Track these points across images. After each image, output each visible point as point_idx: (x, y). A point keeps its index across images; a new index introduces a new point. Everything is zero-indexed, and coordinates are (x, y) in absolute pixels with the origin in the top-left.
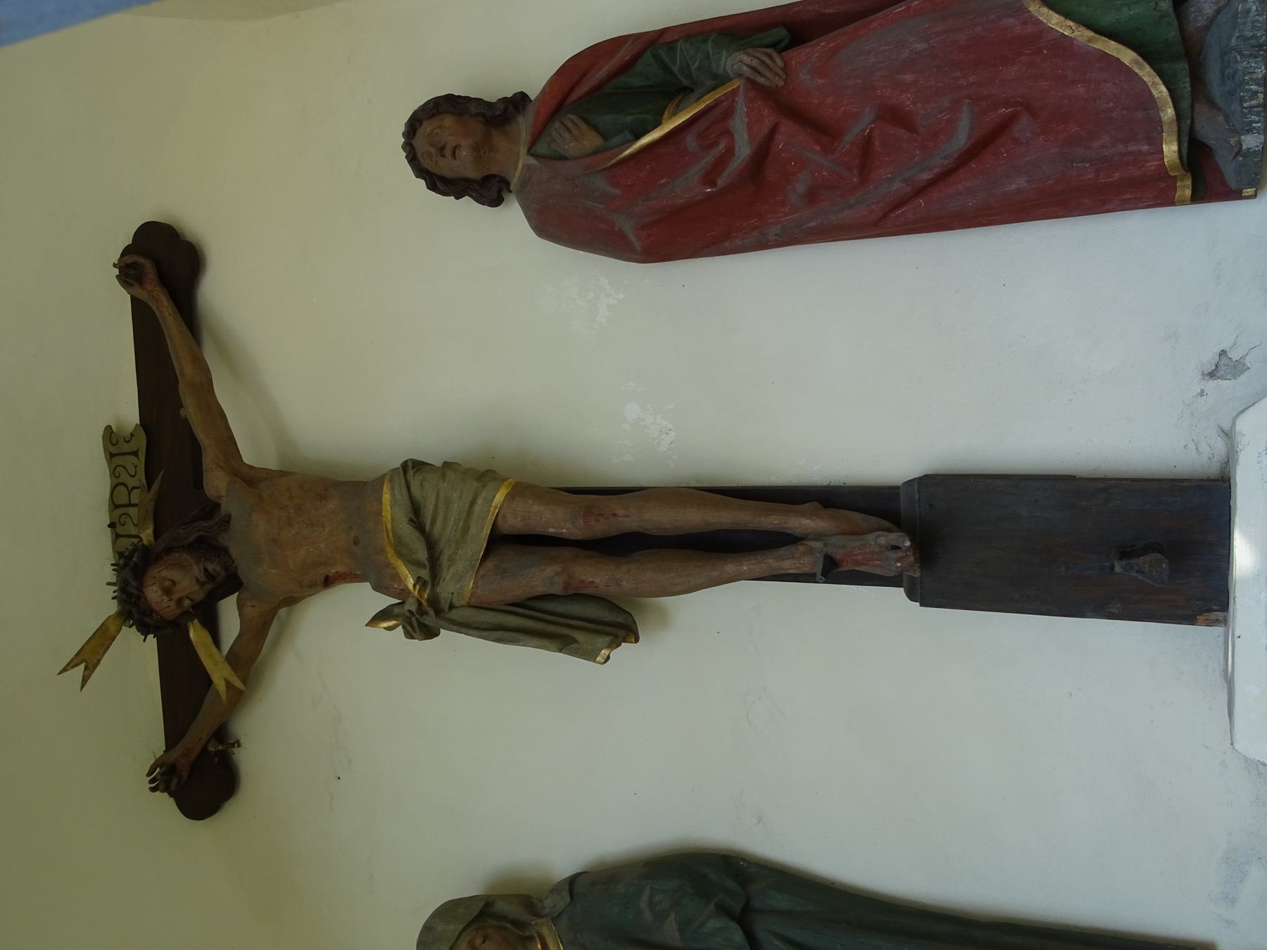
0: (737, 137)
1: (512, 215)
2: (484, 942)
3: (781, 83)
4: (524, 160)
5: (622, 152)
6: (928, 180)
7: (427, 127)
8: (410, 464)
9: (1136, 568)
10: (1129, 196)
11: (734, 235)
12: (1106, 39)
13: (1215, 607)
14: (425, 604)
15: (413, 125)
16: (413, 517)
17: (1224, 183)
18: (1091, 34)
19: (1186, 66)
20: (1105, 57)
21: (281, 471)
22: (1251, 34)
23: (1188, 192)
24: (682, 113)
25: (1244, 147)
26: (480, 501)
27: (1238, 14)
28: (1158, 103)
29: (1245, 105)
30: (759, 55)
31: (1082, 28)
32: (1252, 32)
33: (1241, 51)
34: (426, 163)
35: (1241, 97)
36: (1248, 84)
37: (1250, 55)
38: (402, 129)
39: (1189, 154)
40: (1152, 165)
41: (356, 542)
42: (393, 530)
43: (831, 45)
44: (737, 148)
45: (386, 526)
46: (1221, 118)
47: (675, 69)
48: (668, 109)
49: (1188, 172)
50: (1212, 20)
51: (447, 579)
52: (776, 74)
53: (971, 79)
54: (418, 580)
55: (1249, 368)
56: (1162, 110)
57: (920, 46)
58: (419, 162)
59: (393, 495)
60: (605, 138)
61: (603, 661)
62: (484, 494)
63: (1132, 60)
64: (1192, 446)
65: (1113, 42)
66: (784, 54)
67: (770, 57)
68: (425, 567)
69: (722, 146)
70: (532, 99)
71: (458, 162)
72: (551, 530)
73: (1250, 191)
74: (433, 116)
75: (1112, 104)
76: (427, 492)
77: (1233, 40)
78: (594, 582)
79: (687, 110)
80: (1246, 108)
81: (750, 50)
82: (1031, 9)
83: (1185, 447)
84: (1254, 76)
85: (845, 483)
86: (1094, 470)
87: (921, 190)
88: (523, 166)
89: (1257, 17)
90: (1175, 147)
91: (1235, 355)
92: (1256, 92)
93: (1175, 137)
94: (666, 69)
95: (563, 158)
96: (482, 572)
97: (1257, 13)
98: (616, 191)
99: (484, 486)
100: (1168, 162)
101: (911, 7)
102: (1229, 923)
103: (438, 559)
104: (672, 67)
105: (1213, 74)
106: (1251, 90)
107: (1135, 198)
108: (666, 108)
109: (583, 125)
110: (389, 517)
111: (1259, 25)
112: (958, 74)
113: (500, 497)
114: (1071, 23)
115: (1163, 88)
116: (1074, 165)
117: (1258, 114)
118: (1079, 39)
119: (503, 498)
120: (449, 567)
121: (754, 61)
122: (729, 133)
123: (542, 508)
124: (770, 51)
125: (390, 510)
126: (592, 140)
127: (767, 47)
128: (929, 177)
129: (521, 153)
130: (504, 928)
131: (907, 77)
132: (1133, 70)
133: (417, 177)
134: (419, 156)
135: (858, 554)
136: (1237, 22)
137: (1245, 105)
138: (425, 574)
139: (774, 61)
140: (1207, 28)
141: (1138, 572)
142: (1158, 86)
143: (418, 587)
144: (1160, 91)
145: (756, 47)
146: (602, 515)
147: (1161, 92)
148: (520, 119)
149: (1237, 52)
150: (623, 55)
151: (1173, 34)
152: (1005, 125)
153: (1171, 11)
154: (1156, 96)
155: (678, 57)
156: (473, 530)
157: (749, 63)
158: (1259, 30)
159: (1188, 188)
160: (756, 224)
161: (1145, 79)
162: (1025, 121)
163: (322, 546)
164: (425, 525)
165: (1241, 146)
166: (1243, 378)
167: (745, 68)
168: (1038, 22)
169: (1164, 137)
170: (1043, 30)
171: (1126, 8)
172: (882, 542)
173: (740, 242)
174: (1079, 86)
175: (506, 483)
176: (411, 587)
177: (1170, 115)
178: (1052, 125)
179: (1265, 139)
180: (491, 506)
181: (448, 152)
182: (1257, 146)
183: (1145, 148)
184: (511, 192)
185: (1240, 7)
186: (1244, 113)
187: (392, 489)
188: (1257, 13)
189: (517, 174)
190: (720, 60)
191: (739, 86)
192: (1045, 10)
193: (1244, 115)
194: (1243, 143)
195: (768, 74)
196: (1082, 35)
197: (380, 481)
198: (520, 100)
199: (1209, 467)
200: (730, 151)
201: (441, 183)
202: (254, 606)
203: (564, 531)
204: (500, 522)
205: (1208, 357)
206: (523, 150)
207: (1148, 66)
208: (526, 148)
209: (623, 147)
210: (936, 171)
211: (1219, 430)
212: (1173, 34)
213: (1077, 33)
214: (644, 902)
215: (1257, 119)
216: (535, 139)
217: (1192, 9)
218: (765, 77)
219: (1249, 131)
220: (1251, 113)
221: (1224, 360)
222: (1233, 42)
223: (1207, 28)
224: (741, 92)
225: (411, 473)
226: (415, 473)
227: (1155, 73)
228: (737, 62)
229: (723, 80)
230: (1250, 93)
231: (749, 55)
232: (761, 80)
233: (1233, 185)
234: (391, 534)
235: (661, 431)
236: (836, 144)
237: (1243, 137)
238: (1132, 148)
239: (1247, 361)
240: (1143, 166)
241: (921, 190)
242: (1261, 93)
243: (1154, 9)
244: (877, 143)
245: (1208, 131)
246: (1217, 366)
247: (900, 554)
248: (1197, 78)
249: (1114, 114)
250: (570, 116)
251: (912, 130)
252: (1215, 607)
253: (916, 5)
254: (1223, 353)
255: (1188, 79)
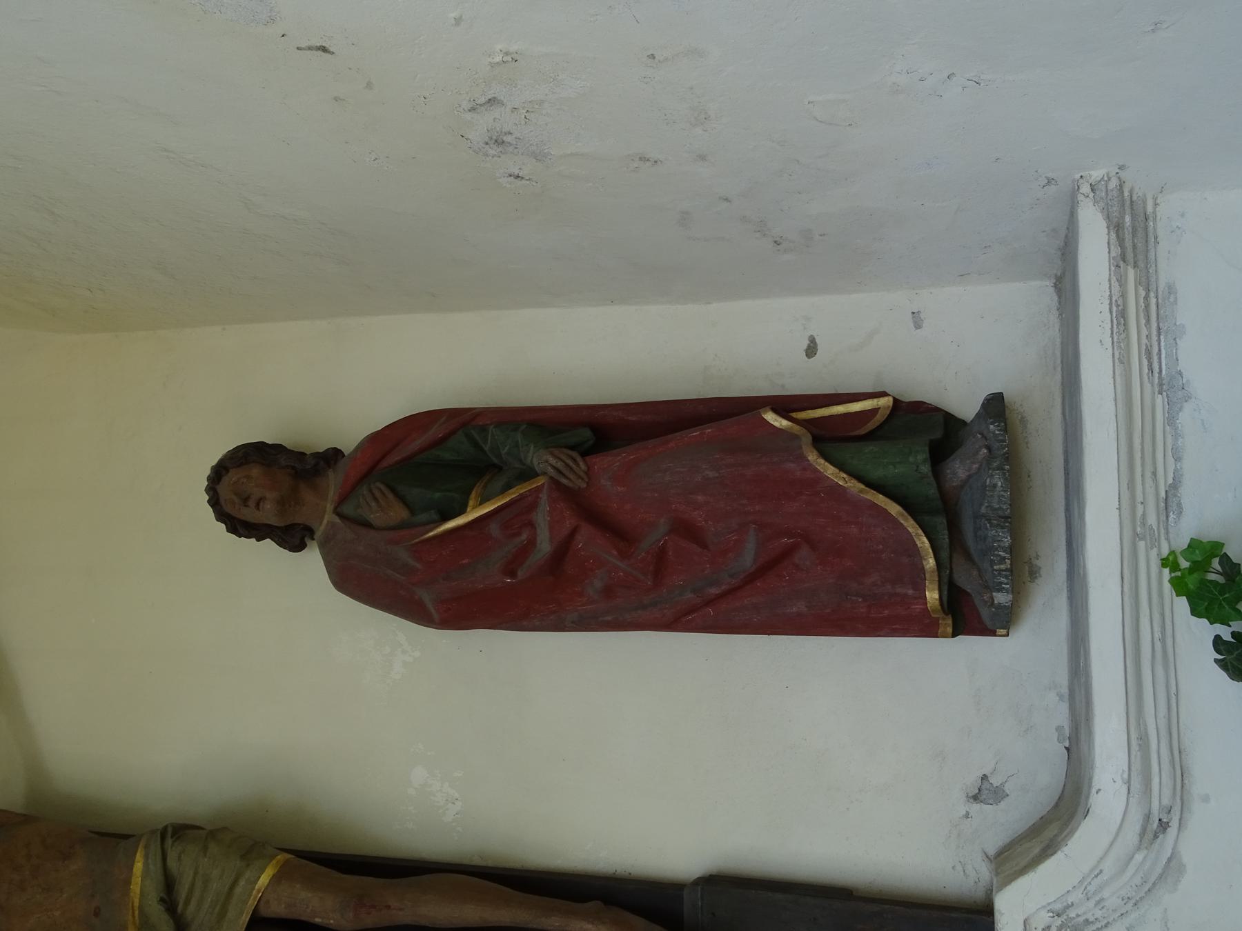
0: (538, 531)
1: (312, 560)
3: (584, 485)
4: (329, 516)
5: (428, 532)
6: (716, 595)
7: (232, 477)
8: (170, 830)
10: (897, 626)
11: (533, 615)
12: (875, 492)
15: (219, 473)
16: (165, 897)
17: (980, 621)
18: (863, 486)
19: (945, 521)
20: (875, 506)
21: (25, 815)
22: (998, 506)
23: (950, 630)
24: (488, 503)
25: (996, 602)
26: (242, 883)
27: (986, 487)
28: (921, 552)
29: (995, 567)
30: (564, 458)
31: (854, 481)
32: (998, 504)
33: (991, 520)
34: (228, 509)
35: (992, 560)
36: (997, 549)
37: (998, 525)
38: (208, 472)
39: (948, 602)
40: (917, 608)
41: (97, 913)
42: (140, 907)
43: (632, 457)
44: (538, 542)
45: (133, 904)
46: (975, 573)
47: (486, 448)
48: (475, 488)
49: (947, 615)
50: (965, 482)
52: (580, 477)
53: (757, 508)
55: (1008, 795)
56: (925, 559)
57: (711, 474)
58: (221, 507)
59: (146, 864)
60: (412, 512)
62: (248, 874)
63: (898, 512)
64: (959, 868)
65: (881, 496)
66: (588, 458)
67: (574, 460)
69: (524, 537)
70: (346, 455)
71: (261, 513)
72: (318, 920)
73: (1003, 631)
74: (240, 465)
75: (881, 547)
76: (185, 862)
77: (983, 508)
79: (492, 501)
80: (996, 571)
81: (556, 452)
82: (809, 458)
83: (953, 868)
84: (1002, 544)
85: (630, 874)
86: (870, 883)
87: (710, 602)
88: (328, 522)
89: (1002, 493)
90: (936, 596)
91: (995, 781)
92: (1004, 558)
93: (936, 587)
94: (476, 445)
95: (367, 525)
97: (1002, 489)
98: (418, 565)
99: (248, 865)
100: (931, 607)
101: (705, 433)
104: (484, 446)
105: (968, 528)
106: (1000, 555)
107: (903, 629)
108: (473, 489)
109: (391, 496)
110: (138, 891)
111: (1003, 499)
112: (745, 502)
113: (264, 880)
114: (845, 476)
115: (925, 540)
116: (849, 597)
117: (1006, 577)
118: (852, 490)
119: (268, 881)
121: (559, 463)
122: (531, 525)
123: (310, 895)
124: (574, 454)
125: (140, 882)
126: (398, 513)
127: (572, 448)
128: (717, 592)
129: (328, 510)
131: (699, 498)
132: (898, 521)
133: (217, 520)
134: (222, 501)
136: (986, 494)
137: (995, 567)
139: (578, 465)
140: (962, 487)
142: (921, 537)
144: (923, 542)
145: (561, 447)
146: (373, 907)
147: (923, 543)
148: (331, 474)
149: (987, 520)
150: (436, 432)
151: (933, 491)
152: (787, 553)
153: (930, 474)
154: (919, 545)
155: (490, 438)
156: (231, 914)
157: (554, 464)
158: (1004, 504)
159: (949, 626)
160: (554, 609)
161: (909, 529)
162: (804, 551)
163: (57, 914)
164: (178, 905)
165: (994, 601)
166: (1002, 805)
167: (550, 470)
168: (816, 470)
169: (927, 584)
170: (820, 478)
171: (891, 467)
173: (538, 623)
174: (853, 526)
175: (274, 862)
177: (932, 565)
178: (829, 558)
179: (1013, 598)
180: (254, 889)
181: (252, 503)
182: (1007, 603)
183: (910, 592)
184: (313, 539)
185: (988, 481)
186: (994, 574)
187: (146, 857)
188: (1002, 489)
189: (322, 528)
190: (528, 452)
191: (544, 483)
192: (822, 461)
193: (995, 576)
194: (995, 599)
195: (572, 476)
196: (854, 487)
197: (142, 836)
198: (333, 456)
199: (975, 891)
200: (532, 543)
201: (239, 527)
203: (332, 921)
205: (971, 779)
206: (330, 507)
207: (912, 519)
208: (333, 506)
209: (428, 527)
210: (723, 587)
211: (983, 854)
212: (932, 491)
213: (849, 484)
215: (1006, 581)
216: (343, 499)
217: (948, 471)
218: (570, 479)
219: (1000, 590)
220: (1000, 575)
221: (986, 785)
222: (983, 510)
223: (962, 487)
224: (545, 491)
225: (169, 841)
226: (174, 842)
227: (917, 526)
228: (542, 459)
229: (527, 474)
230: (999, 558)
231: (552, 454)
232: (564, 481)
233: (988, 623)
235: (447, 800)
236: (632, 550)
237: (994, 594)
238: (899, 590)
239: (1007, 788)
240: (909, 608)
241: (710, 602)
242: (1008, 559)
243: (916, 470)
244: (670, 554)
245: (966, 579)
246: (979, 790)
248: (954, 526)
249: (884, 555)
250: (378, 484)
251: (704, 546)
253: (709, 432)
254: (985, 777)
255: (946, 532)
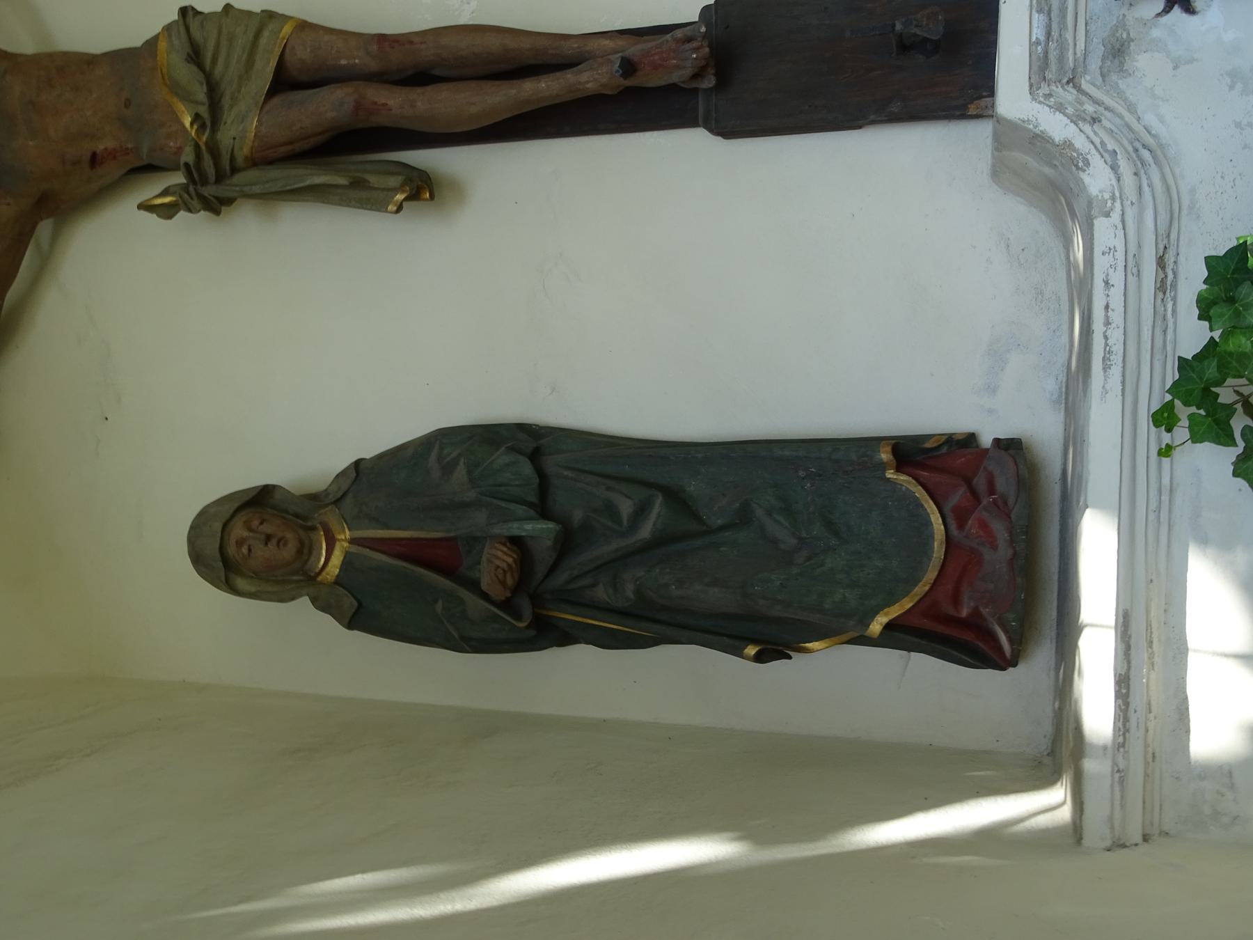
2: (261, 523)
9: (914, 23)
13: (985, 94)
14: (203, 147)
26: (266, 33)
41: (127, 104)
51: (229, 122)
54: (197, 118)
61: (395, 208)
68: (204, 104)
72: (343, 62)
78: (387, 104)
96: (267, 107)
102: (991, 411)
103: (220, 101)
120: (231, 107)
130: (284, 518)
135: (655, 54)
138: (204, 111)
141: (916, 26)
143: (195, 127)
156: (258, 64)
172: (679, 36)
176: (187, 124)
202: (9, 204)
203: (357, 61)
204: (287, 56)
214: (433, 456)
234: (166, 77)
247: (695, 44)
252: (985, 94)
